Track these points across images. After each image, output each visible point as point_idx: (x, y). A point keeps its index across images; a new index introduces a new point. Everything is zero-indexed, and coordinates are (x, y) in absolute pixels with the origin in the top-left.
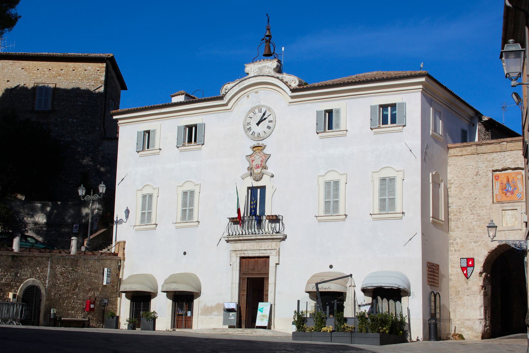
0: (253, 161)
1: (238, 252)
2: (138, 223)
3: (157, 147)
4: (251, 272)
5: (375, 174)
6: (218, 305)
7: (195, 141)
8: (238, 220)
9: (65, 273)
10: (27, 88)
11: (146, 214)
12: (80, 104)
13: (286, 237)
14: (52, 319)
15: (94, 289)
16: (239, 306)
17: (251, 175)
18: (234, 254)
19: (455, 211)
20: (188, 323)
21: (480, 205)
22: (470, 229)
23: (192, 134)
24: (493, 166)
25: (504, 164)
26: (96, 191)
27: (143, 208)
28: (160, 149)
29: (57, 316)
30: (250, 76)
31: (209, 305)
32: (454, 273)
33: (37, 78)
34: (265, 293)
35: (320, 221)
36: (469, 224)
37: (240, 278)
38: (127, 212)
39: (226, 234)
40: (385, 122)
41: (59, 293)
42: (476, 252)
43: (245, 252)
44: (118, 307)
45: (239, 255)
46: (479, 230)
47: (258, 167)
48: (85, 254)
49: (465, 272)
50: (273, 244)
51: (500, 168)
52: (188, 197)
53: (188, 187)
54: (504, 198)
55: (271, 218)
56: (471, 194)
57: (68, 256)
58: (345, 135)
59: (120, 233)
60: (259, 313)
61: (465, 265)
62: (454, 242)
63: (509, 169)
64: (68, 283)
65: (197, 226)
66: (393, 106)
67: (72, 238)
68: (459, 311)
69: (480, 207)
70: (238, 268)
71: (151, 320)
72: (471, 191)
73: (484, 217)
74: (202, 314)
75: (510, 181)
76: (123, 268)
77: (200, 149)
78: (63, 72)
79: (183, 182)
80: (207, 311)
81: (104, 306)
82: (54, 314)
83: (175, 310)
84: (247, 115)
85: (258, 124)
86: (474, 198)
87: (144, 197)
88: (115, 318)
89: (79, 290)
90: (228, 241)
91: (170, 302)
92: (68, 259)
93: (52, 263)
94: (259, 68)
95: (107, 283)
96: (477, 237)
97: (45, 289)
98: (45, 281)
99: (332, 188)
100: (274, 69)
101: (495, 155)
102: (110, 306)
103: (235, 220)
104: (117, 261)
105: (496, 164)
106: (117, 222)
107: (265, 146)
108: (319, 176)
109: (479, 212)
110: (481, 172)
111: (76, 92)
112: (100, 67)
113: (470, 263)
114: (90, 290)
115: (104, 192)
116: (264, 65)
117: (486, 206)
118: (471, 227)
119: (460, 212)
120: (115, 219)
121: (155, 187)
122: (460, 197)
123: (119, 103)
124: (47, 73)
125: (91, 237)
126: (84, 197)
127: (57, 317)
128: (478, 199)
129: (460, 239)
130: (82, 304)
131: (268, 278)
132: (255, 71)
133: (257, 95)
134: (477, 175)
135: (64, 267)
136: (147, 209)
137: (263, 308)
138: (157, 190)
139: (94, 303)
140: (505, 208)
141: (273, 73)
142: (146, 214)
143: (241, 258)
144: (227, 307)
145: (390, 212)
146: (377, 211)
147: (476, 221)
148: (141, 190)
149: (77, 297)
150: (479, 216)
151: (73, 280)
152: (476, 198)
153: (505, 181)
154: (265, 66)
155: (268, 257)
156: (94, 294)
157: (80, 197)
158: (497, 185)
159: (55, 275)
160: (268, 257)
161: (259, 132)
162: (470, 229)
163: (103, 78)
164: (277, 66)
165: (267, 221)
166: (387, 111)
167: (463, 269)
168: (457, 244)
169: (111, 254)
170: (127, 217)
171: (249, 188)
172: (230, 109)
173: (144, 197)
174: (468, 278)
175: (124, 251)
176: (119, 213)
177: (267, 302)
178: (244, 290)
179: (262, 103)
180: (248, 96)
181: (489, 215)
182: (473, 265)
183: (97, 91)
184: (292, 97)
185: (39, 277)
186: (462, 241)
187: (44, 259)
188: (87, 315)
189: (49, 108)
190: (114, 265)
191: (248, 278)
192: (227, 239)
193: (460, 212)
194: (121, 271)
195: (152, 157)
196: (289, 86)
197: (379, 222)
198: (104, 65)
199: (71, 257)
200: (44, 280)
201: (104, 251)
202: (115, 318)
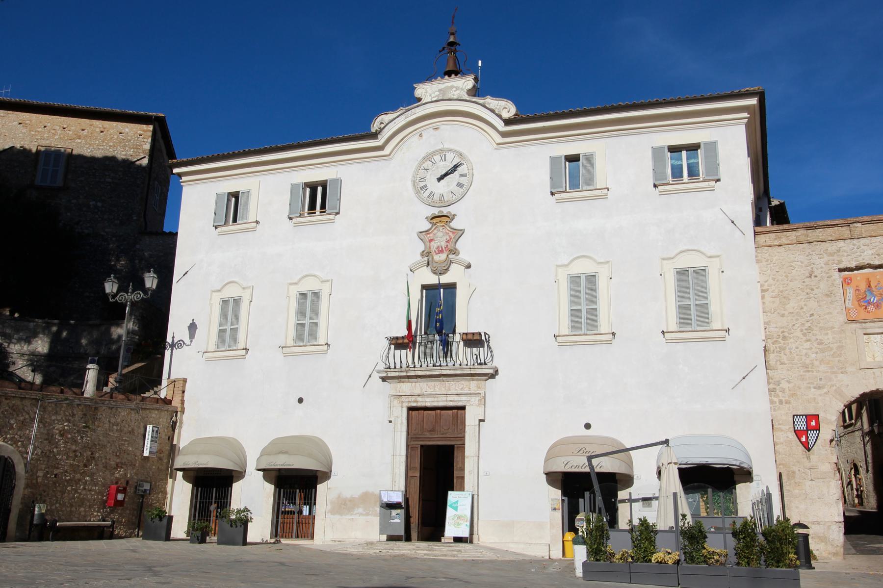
0: (431, 241)
1: (403, 399)
2: (212, 347)
3: (251, 218)
4: (428, 435)
5: (665, 262)
6: (365, 497)
7: (323, 206)
8: (406, 341)
9: (68, 432)
10: (30, 151)
11: (228, 332)
12: (110, 180)
13: (497, 372)
14: (36, 525)
15: (125, 464)
16: (407, 500)
17: (428, 264)
18: (396, 402)
19: (775, 335)
20: (305, 528)
21: (820, 325)
22: (805, 366)
23: (317, 198)
24: (840, 262)
25: (860, 259)
26: (140, 285)
27: (223, 321)
28: (257, 222)
29: (48, 517)
30: (423, 101)
31: (347, 494)
32: (782, 440)
33: (43, 138)
34: (456, 474)
35: (561, 344)
36: (803, 358)
37: (408, 445)
38: (193, 327)
39: (381, 367)
40: (677, 173)
41: (56, 472)
42: (820, 404)
43: (419, 399)
44: (169, 496)
45: (406, 405)
46: (823, 368)
47: (442, 251)
48: (111, 397)
49: (803, 439)
50: (472, 385)
51: (853, 265)
52: (308, 303)
53: (308, 286)
54: (863, 315)
55: (470, 337)
56: (802, 308)
57: (79, 399)
58: (605, 197)
59: (178, 364)
60: (450, 512)
61: (802, 425)
62: (778, 388)
63: (870, 266)
64: (75, 451)
65: (325, 352)
66: (693, 148)
67: (89, 366)
68: (797, 507)
69: (821, 329)
70: (404, 428)
71: (238, 525)
72: (802, 303)
73: (831, 346)
74: (333, 512)
75: (873, 285)
76: (181, 427)
77: (332, 221)
78: (85, 132)
79: (300, 277)
80: (344, 506)
81: (143, 496)
82: (42, 515)
83: (279, 503)
84: (420, 165)
85: (440, 179)
86: (808, 315)
87: (225, 302)
88: (165, 521)
89: (96, 465)
90: (384, 379)
91: (270, 488)
92: (78, 405)
93: (44, 411)
94: (440, 90)
95: (150, 453)
96: (821, 379)
97: (25, 465)
98: (25, 447)
99: (584, 288)
100: (468, 91)
101: (841, 244)
102: (153, 497)
103: (400, 341)
104: (170, 413)
105: (843, 259)
106: (173, 346)
107: (454, 215)
108: (558, 266)
109: (819, 337)
110: (817, 272)
111: (110, 162)
112: (144, 131)
113: (813, 423)
114: (118, 466)
115: (154, 287)
116: (449, 84)
117: (832, 328)
118: (808, 362)
119: (784, 338)
120: (169, 339)
121: (245, 285)
122: (783, 312)
123: (168, 191)
124: (59, 132)
125: (125, 371)
126: (114, 296)
127: (46, 521)
128: (815, 316)
129: (789, 382)
130: (100, 493)
131: (462, 447)
132: (433, 95)
133: (436, 132)
134: (810, 276)
135: (69, 421)
136: (229, 323)
137: (457, 504)
138: (249, 291)
139: (124, 491)
140: (869, 331)
141: (466, 97)
142: (228, 332)
143: (411, 409)
144: (385, 499)
145: (699, 329)
146: (673, 326)
147: (817, 353)
148: (219, 291)
149: (92, 480)
150: (820, 343)
151: (86, 447)
152: (812, 315)
153: (863, 287)
154: (452, 87)
155: (463, 408)
156: (126, 475)
157: (106, 296)
158: (850, 292)
159: (49, 438)
160: (463, 408)
161: (441, 192)
162: (805, 366)
163: (147, 147)
164: (474, 86)
165: (462, 343)
166: (681, 160)
167: (798, 433)
168: (783, 391)
169: (158, 400)
170: (192, 336)
171: (424, 287)
172: (389, 155)
173: (225, 302)
174: (809, 450)
175: (183, 397)
176: (176, 328)
177: (462, 489)
178: (415, 468)
179: (446, 146)
180: (421, 135)
181: (840, 342)
182: (817, 428)
183: (138, 163)
184: (504, 135)
185: (12, 439)
186: (791, 385)
187: (27, 403)
188: (110, 513)
189: (60, 182)
190: (164, 420)
191: (422, 446)
192: (384, 375)
193: (784, 338)
194: (177, 431)
195: (241, 236)
196: (500, 116)
197: (679, 347)
198: (151, 127)
199: (84, 402)
200: (23, 445)
201: (147, 395)
202: (165, 521)
